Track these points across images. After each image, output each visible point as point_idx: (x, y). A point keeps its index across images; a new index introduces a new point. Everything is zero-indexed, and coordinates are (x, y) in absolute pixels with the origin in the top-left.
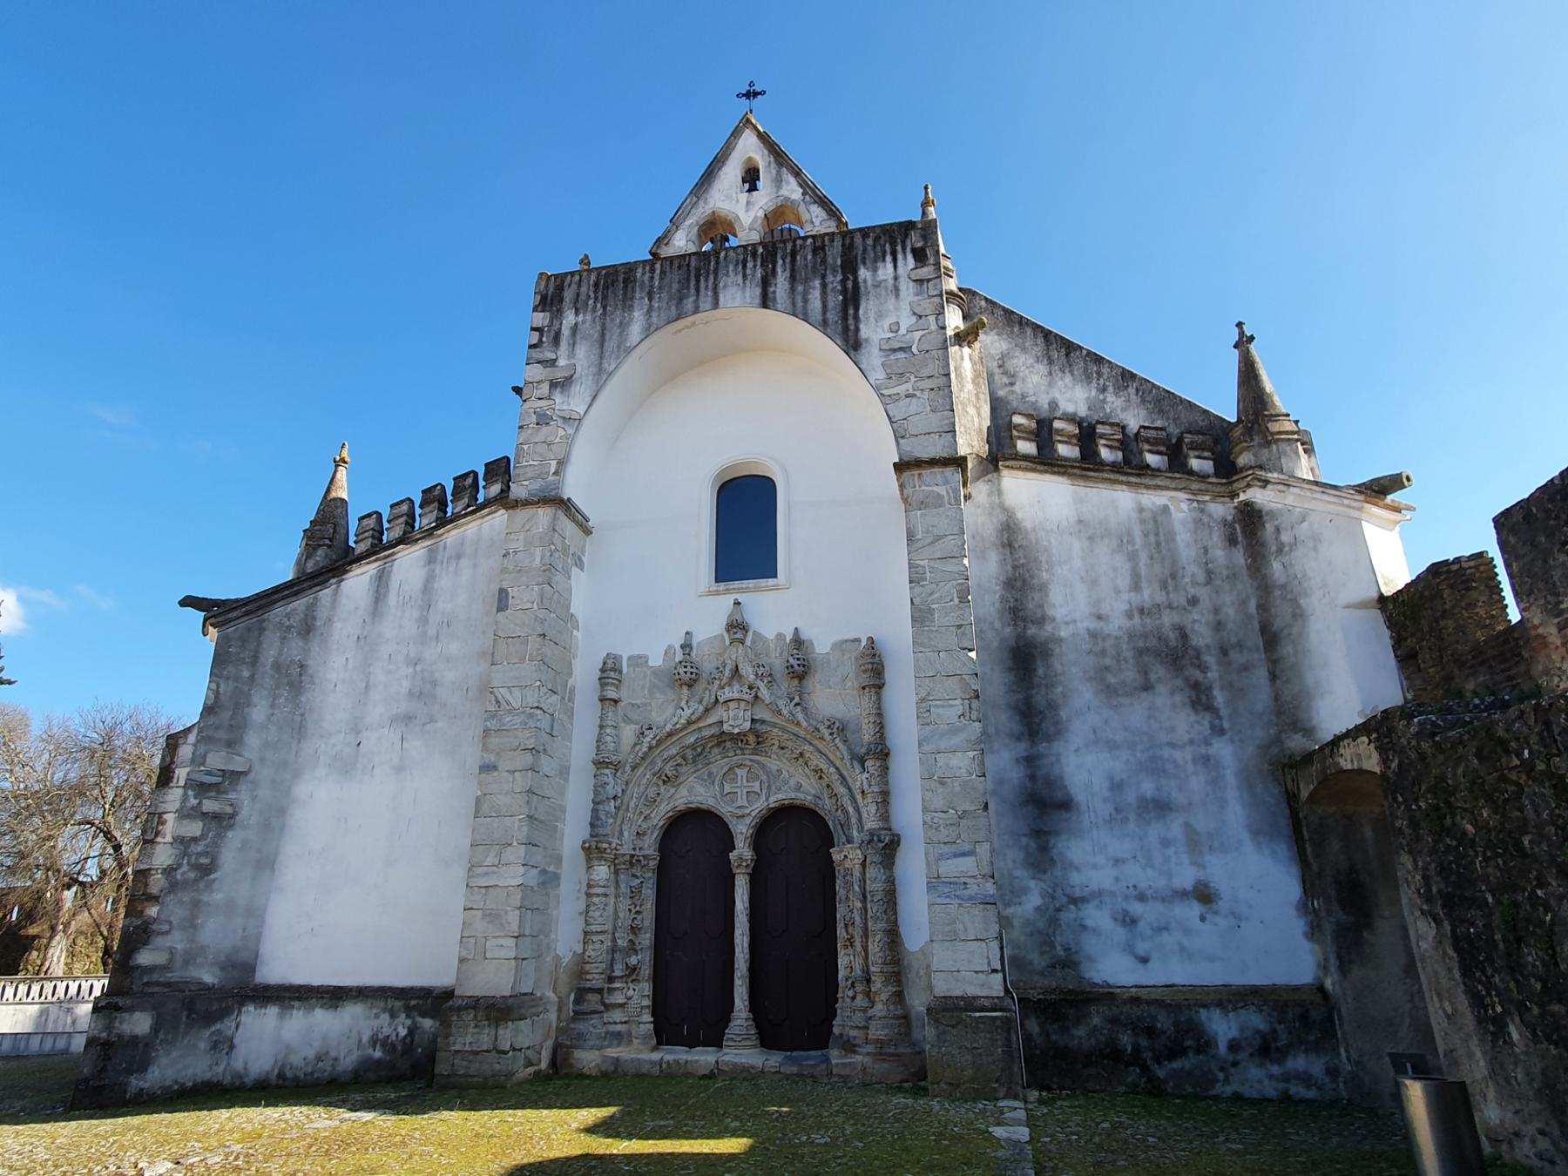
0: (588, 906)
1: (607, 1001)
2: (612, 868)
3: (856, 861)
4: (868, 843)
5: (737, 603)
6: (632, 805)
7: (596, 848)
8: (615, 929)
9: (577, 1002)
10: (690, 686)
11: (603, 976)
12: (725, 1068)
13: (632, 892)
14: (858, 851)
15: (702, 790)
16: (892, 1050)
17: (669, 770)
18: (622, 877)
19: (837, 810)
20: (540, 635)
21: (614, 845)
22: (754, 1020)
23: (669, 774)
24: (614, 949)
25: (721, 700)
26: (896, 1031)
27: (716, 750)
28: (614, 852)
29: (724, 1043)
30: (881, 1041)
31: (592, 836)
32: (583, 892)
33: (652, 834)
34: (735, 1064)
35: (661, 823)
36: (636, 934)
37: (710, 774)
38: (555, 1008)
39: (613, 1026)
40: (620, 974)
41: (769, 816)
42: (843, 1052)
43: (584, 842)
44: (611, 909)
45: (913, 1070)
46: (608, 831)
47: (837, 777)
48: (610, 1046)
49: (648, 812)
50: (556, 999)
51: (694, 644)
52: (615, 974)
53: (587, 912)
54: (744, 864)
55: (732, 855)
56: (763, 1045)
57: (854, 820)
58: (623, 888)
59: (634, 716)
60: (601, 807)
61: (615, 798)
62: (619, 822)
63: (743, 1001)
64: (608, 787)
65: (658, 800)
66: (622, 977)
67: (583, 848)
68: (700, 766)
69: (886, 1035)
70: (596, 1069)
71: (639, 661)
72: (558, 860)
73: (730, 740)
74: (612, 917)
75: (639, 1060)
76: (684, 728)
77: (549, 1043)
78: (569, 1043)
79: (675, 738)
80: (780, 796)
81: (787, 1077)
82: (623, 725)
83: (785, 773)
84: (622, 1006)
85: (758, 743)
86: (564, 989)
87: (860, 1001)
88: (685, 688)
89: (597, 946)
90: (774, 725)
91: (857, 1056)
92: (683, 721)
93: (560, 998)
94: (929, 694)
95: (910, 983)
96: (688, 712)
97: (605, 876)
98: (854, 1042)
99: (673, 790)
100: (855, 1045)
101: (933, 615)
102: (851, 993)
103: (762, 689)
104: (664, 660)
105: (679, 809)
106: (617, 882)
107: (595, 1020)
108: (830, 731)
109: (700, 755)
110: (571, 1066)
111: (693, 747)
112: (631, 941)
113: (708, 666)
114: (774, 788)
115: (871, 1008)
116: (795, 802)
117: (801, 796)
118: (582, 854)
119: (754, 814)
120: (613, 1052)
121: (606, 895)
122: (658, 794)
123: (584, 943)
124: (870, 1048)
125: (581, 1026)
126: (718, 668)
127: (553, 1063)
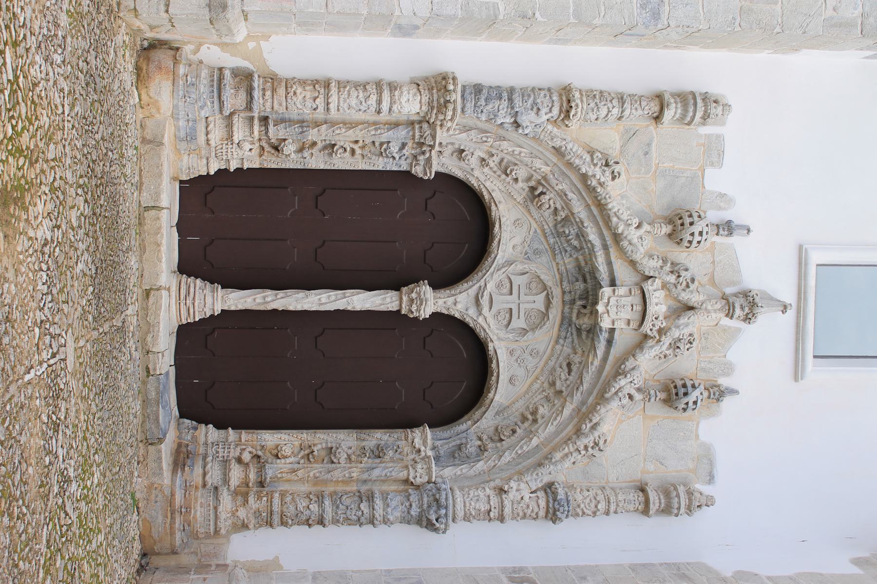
1: (235, 118)
2: (416, 118)
5: (785, 308)
8: (332, 124)
11: (269, 110)
13: (382, 144)
14: (426, 479)
22: (212, 316)
23: (545, 199)
30: (188, 512)
36: (325, 148)
39: (204, 129)
44: (361, 116)
49: (492, 164)
55: (425, 289)
64: (533, 114)
65: (509, 179)
74: (347, 118)
76: (609, 227)
82: (621, 128)
84: (230, 137)
89: (309, 103)
99: (520, 199)
103: (657, 348)
105: (493, 208)
111: (581, 235)
119: (481, 320)
121: (379, 112)
122: (516, 180)
126: (693, 280)
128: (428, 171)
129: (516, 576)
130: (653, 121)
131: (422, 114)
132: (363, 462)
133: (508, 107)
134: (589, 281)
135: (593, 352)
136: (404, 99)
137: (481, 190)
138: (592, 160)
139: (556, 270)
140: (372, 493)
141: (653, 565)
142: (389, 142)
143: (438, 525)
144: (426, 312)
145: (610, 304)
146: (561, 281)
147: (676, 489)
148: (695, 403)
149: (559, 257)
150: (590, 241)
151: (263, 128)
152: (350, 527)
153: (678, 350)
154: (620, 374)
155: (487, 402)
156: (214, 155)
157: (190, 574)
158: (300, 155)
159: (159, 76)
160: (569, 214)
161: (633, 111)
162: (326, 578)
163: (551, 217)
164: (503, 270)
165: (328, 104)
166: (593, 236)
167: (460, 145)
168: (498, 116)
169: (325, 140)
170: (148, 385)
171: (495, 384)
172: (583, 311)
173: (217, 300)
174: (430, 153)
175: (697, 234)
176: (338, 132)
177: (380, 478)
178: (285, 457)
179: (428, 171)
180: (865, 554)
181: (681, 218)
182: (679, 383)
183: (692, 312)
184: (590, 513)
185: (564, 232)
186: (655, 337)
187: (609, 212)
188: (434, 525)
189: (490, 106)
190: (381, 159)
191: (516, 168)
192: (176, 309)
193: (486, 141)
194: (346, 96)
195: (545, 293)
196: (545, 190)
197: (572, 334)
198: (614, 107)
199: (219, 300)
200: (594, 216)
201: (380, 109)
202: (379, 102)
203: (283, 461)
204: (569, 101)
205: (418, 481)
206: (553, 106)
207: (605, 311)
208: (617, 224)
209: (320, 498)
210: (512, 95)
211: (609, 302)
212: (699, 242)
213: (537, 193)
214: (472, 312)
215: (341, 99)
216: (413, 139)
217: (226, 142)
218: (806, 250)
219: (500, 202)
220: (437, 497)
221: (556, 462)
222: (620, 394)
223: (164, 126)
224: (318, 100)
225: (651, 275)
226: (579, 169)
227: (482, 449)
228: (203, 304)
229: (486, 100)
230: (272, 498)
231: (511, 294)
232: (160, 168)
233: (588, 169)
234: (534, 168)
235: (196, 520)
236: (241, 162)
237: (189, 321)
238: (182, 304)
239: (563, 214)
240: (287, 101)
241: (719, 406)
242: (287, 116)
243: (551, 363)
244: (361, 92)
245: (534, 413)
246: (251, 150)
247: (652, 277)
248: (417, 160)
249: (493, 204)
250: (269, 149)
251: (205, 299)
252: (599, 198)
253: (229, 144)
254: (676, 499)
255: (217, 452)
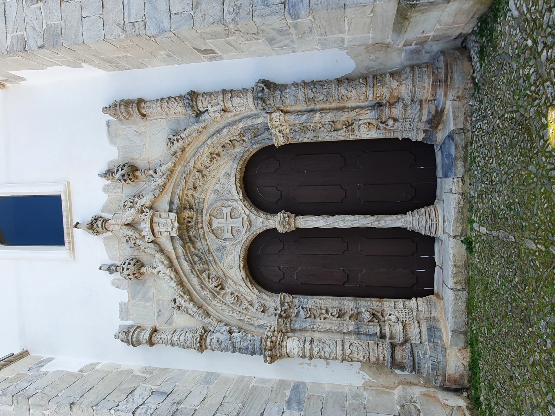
0: (320, 357)
1: (401, 340)
2: (290, 334)
3: (282, 118)
4: (264, 102)
6: (238, 317)
7: (271, 350)
8: (341, 332)
9: (402, 367)
10: (143, 265)
12: (460, 229)
13: (310, 317)
14: (274, 115)
15: (230, 257)
16: (442, 71)
17: (212, 285)
18: (297, 326)
19: (244, 141)
20: (71, 408)
21: (270, 334)
22: (412, 211)
23: (215, 284)
24: (358, 333)
25: (152, 238)
26: (425, 69)
27: (198, 245)
28: (276, 333)
29: (432, 235)
30: (434, 82)
31: (261, 354)
32: (309, 362)
33: (264, 299)
34: (457, 221)
35: (256, 291)
36: (344, 314)
37: (218, 250)
38: (409, 389)
39: (423, 335)
40: (378, 328)
41: (250, 199)
42: (440, 127)
43: (266, 361)
45: (458, 54)
46: (258, 339)
47: (215, 137)
48: (441, 338)
49: (246, 303)
50: (400, 386)
51: (110, 262)
52: (378, 333)
53: (326, 358)
54: (287, 219)
55: (281, 230)
56: (432, 203)
57: (249, 122)
58: (307, 324)
59: (167, 315)
60: (238, 345)
61: (230, 332)
62: (252, 328)
63: (398, 219)
64: (221, 339)
65: (236, 294)
66: (380, 326)
67: (271, 362)
68: (211, 258)
69: (429, 78)
70: (463, 351)
71: (124, 311)
72: (282, 383)
73: (188, 231)
74: (331, 335)
75: (454, 311)
76: (177, 272)
77: (441, 395)
78: (440, 378)
79: (184, 279)
80: (234, 190)
81: (468, 170)
82: (174, 325)
83: (217, 187)
85: (191, 208)
86: (392, 380)
87: (397, 112)
88: (143, 270)
89: (355, 350)
90: (173, 193)
91: (447, 107)
92: (168, 271)
93: (399, 384)
94: (118, 25)
95: (381, 67)
96: (161, 267)
97: (296, 342)
98: (434, 113)
99: (230, 282)
100: (436, 111)
101: (51, 26)
102: (391, 122)
104: (123, 289)
105: (244, 277)
106: (301, 330)
107: (419, 352)
108: (175, 142)
109: (200, 258)
110: (462, 376)
111: (192, 264)
112: (350, 318)
113: (127, 252)
114: (228, 196)
115: (403, 100)
116: (238, 177)
117: (234, 171)
118: (277, 362)
119: (248, 212)
120: (447, 336)
122: (232, 294)
123: (352, 361)
124: (441, 91)
125: (426, 366)
126: (127, 241)
127: (457, 391)
128: (282, 299)
129: (211, 55)
130: (157, 329)
131: (286, 337)
132: (314, 123)
133: (236, 342)
134: (187, 237)
135: (181, 197)
136: (297, 350)
137: (252, 286)
138: (187, 310)
139: (208, 241)
140: (306, 104)
141: (134, 68)
142: (306, 318)
143: (263, 85)
144: (280, 216)
145: (171, 227)
146: (204, 235)
147: (125, 117)
148: (118, 170)
149: (206, 249)
150: (187, 261)
151: (383, 332)
152: (320, 80)
153: (132, 201)
154: (162, 186)
155: (241, 163)
156: (414, 313)
157: (433, 36)
158: (359, 310)
159: (456, 377)
160: (200, 276)
161: (166, 338)
162: (335, 43)
163: (211, 272)
164: (237, 241)
165: (343, 350)
166: (186, 265)
167: (264, 315)
168: (241, 338)
169: (344, 320)
170: (463, 171)
171: (237, 174)
172: (190, 220)
173: (410, 222)
174: (281, 309)
175: (125, 269)
176: (336, 328)
177: (302, 113)
178: (365, 124)
179: (282, 299)
180: (21, 83)
181: (136, 277)
182: (129, 181)
183: (125, 223)
184: (172, 99)
185: (203, 265)
186: (145, 208)
187: (176, 280)
188: (265, 85)
189: (245, 344)
190: (310, 307)
191: (232, 302)
192: (438, 217)
193: (249, 319)
194: (331, 354)
195: (212, 229)
196: (215, 289)
197: (195, 205)
198: (177, 341)
199: (409, 222)
200: (185, 276)
201: (311, 343)
202: (311, 349)
203: (366, 121)
204: (201, 346)
205: (278, 114)
206: (210, 343)
207: (174, 223)
208: (170, 273)
209: (340, 98)
210: (233, 350)
211: (172, 229)
212: (124, 264)
213: (220, 287)
214: (253, 217)
215: (335, 352)
216: (291, 321)
217: (407, 322)
218: (71, 257)
219: (241, 280)
220: (264, 104)
221: (195, 131)
222: (161, 174)
223: (451, 342)
224: (349, 353)
225: (150, 244)
226: (194, 305)
227: (241, 135)
228: (420, 221)
229: (248, 348)
230: (374, 96)
231: (231, 227)
232: (454, 316)
233: (189, 306)
234: (221, 302)
235: (428, 76)
236: (396, 306)
237: (429, 209)
238: (435, 220)
239: (204, 275)
240: (369, 352)
241: (108, 167)
242: (368, 337)
243: (206, 187)
244: (323, 356)
245: (212, 159)
246: (390, 315)
247: (150, 242)
248: (289, 305)
249: (245, 279)
250: (378, 314)
251: (419, 223)
252: (181, 289)
253: (404, 321)
254: (122, 111)
255: (410, 124)
